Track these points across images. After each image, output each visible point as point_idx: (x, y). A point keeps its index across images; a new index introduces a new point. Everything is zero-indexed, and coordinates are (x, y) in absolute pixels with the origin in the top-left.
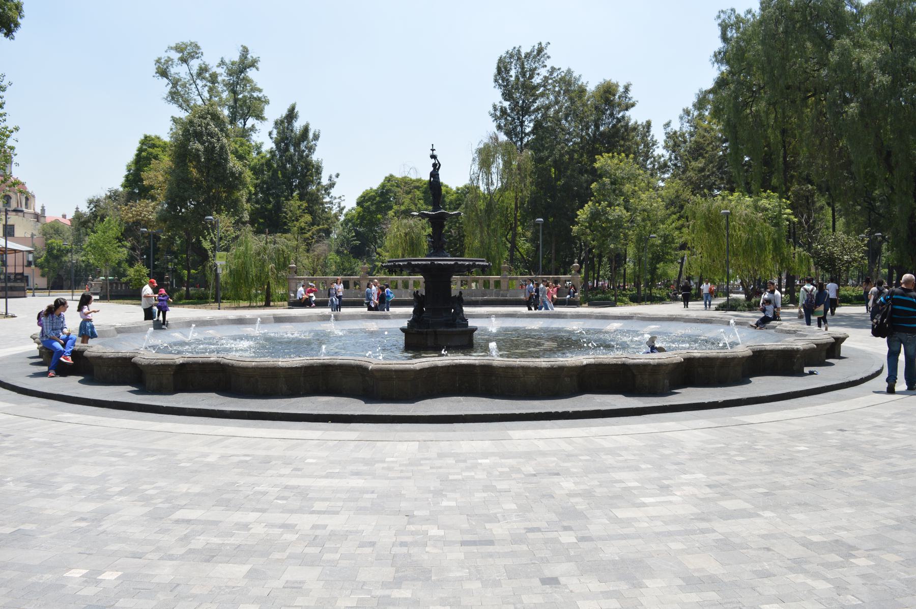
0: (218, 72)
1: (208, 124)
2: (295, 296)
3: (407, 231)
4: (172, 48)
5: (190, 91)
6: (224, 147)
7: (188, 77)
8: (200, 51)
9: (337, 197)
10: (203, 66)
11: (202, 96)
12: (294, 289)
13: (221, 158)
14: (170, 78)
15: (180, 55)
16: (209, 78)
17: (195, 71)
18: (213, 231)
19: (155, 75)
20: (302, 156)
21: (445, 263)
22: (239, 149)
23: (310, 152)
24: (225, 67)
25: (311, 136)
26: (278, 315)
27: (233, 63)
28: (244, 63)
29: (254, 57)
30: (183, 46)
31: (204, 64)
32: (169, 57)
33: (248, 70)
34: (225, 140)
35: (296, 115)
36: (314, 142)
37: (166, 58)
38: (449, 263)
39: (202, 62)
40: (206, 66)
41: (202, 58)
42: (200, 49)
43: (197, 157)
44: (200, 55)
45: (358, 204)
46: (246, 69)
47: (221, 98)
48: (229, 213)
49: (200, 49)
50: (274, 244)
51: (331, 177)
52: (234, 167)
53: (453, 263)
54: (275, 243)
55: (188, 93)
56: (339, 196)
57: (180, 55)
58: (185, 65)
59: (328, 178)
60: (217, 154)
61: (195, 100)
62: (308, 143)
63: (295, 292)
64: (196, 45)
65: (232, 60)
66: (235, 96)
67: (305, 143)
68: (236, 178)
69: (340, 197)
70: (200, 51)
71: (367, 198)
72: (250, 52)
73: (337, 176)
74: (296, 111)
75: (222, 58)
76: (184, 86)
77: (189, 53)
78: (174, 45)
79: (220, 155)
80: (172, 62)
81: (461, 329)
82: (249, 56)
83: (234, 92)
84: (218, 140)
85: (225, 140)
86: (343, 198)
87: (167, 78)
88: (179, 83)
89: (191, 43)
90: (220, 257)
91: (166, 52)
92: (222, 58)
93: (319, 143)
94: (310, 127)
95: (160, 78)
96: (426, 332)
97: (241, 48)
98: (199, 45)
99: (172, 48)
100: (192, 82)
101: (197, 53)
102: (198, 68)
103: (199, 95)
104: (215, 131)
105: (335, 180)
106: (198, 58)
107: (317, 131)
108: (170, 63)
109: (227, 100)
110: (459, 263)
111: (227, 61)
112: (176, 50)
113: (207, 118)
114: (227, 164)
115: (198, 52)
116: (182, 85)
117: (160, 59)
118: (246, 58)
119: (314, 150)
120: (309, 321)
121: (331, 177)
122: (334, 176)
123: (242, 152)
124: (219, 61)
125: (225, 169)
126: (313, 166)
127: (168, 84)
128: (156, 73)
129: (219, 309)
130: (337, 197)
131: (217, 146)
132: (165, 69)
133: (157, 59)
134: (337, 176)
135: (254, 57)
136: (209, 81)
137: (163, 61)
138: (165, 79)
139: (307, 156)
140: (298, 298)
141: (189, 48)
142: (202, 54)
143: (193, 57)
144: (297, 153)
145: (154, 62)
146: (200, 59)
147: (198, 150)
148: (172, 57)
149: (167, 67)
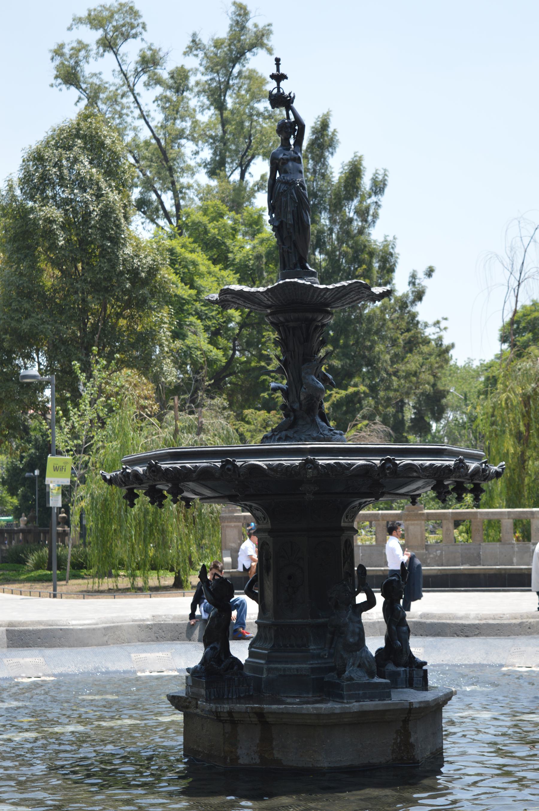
0: (187, 67)
1: (76, 160)
2: (234, 564)
3: (530, 388)
4: (80, 21)
5: (125, 111)
6: (113, 211)
7: (119, 80)
8: (140, 21)
9: (431, 322)
10: (149, 53)
11: (149, 120)
12: (233, 545)
13: (104, 237)
14: (84, 86)
15: (99, 34)
16: (171, 82)
17: (130, 67)
18: (76, 405)
19: (53, 81)
20: (348, 233)
21: (275, 461)
22: (210, 226)
23: (366, 221)
24: (201, 54)
25: (366, 182)
26: (20, 624)
27: (218, 44)
28: (239, 41)
29: (261, 26)
30: (106, 14)
31: (150, 49)
32: (80, 42)
33: (248, 55)
34: (114, 196)
35: (332, 140)
36: (374, 199)
37: (75, 45)
38: (286, 462)
39: (144, 46)
40: (155, 53)
41: (145, 35)
42: (140, 16)
43: (49, 234)
44: (139, 29)
45: (504, 339)
46: (244, 54)
47: (195, 123)
48: (109, 362)
49: (140, 16)
50: (198, 434)
51: (414, 276)
52: (137, 256)
53: (297, 461)
54: (200, 430)
55: (121, 116)
56: (435, 320)
57: (99, 34)
58: (109, 56)
59: (407, 279)
60: (94, 226)
61: (135, 129)
62: (361, 202)
63: (235, 553)
64: (131, 8)
65: (215, 38)
66: (221, 114)
67: (355, 202)
68: (145, 282)
69: (438, 322)
70: (140, 21)
71: (523, 325)
72: (251, 15)
73: (430, 272)
74: (331, 129)
75: (194, 35)
76: (113, 100)
77: (116, 29)
78: (84, 14)
79: (103, 230)
80: (87, 51)
81: (355, 706)
82: (249, 25)
83: (220, 106)
84: (99, 196)
85: (114, 196)
86: (443, 324)
87: (78, 87)
88: (102, 96)
89: (121, 5)
90: (56, 469)
91: (70, 29)
92: (194, 35)
93: (385, 199)
94: (365, 163)
95: (64, 87)
96: (230, 713)
97: (233, 9)
98: (137, 7)
99: (80, 21)
100: (125, 88)
101: (133, 28)
102: (138, 59)
103: (143, 116)
104: (92, 175)
105: (423, 281)
106: (135, 36)
107: (381, 172)
108: (82, 53)
109: (209, 126)
110: (322, 461)
111: (206, 40)
112: (91, 23)
113: (74, 145)
114: (119, 248)
115: (136, 23)
116: (108, 99)
117: (61, 46)
118: (243, 28)
119: (375, 216)
120: (106, 644)
121: (414, 276)
122: (421, 275)
123: (216, 231)
124: (187, 41)
125: (113, 262)
126: (371, 254)
127: (80, 98)
128: (56, 77)
129: (55, 596)
130: (431, 322)
131: (95, 209)
132: (74, 68)
133: (56, 47)
134: (430, 272)
135: (261, 26)
136: (170, 88)
137: (67, 51)
138: (73, 88)
139: (361, 231)
140: (241, 569)
141: (116, 16)
142: (144, 28)
143: (126, 37)
144: (336, 228)
145: (50, 55)
146: (139, 39)
147: (50, 221)
148: (86, 41)
149: (76, 62)
